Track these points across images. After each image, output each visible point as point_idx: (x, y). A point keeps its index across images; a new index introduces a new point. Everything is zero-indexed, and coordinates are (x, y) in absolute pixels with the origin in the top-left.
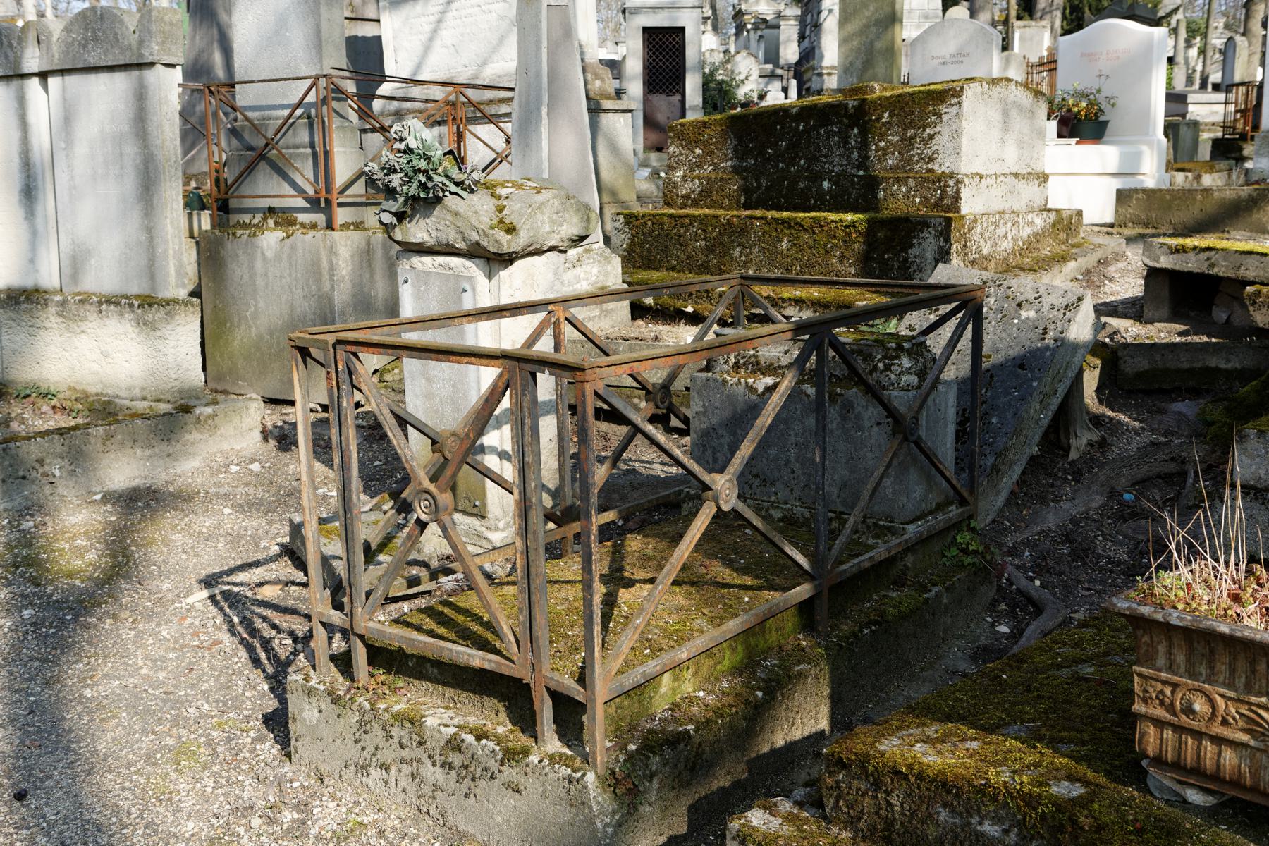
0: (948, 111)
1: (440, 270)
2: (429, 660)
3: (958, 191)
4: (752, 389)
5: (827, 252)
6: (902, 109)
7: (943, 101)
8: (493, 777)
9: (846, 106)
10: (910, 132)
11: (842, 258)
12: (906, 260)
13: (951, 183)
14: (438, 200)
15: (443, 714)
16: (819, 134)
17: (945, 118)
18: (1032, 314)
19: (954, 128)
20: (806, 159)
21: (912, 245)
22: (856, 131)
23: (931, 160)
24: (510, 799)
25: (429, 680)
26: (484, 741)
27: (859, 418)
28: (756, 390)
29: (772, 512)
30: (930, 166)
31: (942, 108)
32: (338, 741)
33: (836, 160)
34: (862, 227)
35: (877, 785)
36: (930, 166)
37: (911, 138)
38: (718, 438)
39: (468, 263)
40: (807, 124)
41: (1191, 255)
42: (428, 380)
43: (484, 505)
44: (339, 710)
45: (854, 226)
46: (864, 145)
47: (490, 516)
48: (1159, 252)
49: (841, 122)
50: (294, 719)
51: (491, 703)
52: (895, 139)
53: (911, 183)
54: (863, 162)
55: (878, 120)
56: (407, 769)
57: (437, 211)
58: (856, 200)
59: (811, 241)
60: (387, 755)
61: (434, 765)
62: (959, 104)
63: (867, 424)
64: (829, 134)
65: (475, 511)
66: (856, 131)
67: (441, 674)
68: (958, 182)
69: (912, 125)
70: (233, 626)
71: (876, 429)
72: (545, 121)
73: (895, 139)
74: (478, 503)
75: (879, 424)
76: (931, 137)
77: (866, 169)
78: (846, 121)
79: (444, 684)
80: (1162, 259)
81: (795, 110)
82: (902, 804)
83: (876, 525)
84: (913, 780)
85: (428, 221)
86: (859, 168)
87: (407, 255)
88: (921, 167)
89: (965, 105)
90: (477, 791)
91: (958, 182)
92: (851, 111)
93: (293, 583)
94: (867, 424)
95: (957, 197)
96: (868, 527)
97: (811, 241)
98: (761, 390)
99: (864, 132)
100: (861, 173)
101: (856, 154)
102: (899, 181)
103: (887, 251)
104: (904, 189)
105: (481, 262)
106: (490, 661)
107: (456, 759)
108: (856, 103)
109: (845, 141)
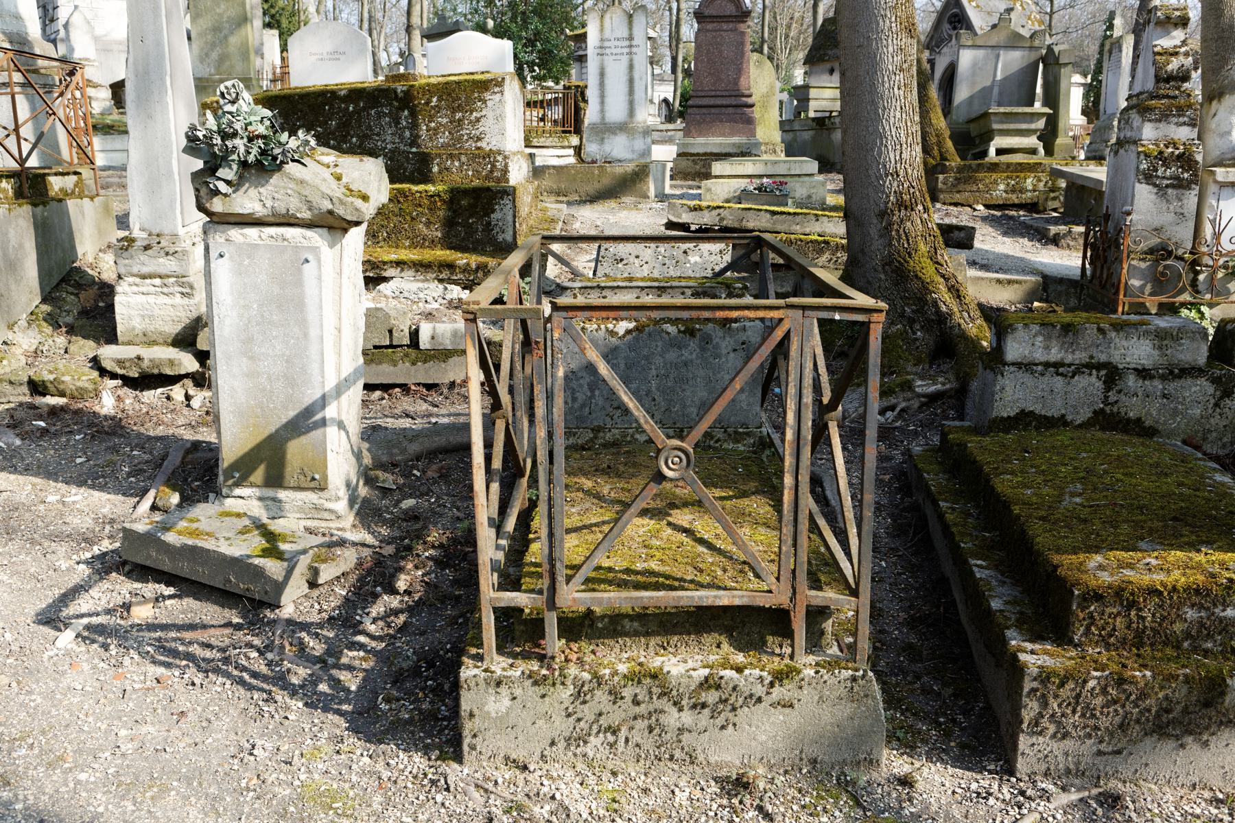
0: (492, 98)
1: (273, 242)
2: (627, 616)
3: (506, 165)
4: (612, 333)
5: (413, 219)
6: (449, 95)
7: (487, 89)
8: (759, 700)
9: (395, 91)
10: (458, 115)
11: (428, 224)
12: (489, 223)
13: (500, 158)
14: (279, 168)
15: (683, 663)
16: (369, 114)
17: (489, 103)
18: (697, 259)
19: (498, 112)
20: (358, 136)
21: (493, 211)
22: (406, 112)
23: (479, 139)
24: (779, 715)
25: (627, 634)
26: (747, 672)
27: (717, 347)
28: (617, 333)
29: (637, 436)
30: (479, 144)
31: (487, 96)
32: (540, 723)
33: (389, 138)
34: (446, 197)
35: (1132, 604)
36: (479, 144)
37: (459, 120)
38: (577, 380)
39: (309, 233)
40: (356, 105)
41: (706, 212)
42: (251, 358)
43: (325, 477)
44: (541, 690)
45: (439, 196)
46: (414, 126)
47: (330, 487)
48: (681, 211)
49: (391, 105)
50: (472, 715)
51: (709, 639)
52: (445, 120)
53: (463, 158)
54: (414, 141)
55: (427, 103)
56: (641, 724)
57: (275, 179)
58: (412, 173)
59: (396, 210)
60: (615, 716)
61: (681, 710)
62: (502, 92)
63: (724, 351)
64: (380, 115)
65: (313, 485)
66: (406, 112)
67: (642, 626)
68: (505, 158)
69: (459, 108)
70: (152, 657)
71: (732, 355)
72: (170, 92)
73: (445, 120)
74: (317, 477)
75: (735, 350)
76: (478, 120)
77: (419, 146)
78: (396, 104)
79: (647, 634)
80: (684, 215)
81: (343, 93)
82: (1154, 615)
83: (736, 432)
84: (1166, 594)
85: (261, 190)
86: (411, 145)
87: (221, 227)
88: (471, 145)
89: (506, 93)
90: (736, 720)
91: (505, 158)
92: (401, 95)
93: (164, 598)
94: (724, 351)
95: (505, 171)
96: (730, 435)
97: (396, 210)
98: (621, 333)
99: (413, 114)
100: (414, 150)
101: (407, 134)
102: (451, 157)
103: (471, 216)
104: (457, 164)
105: (324, 231)
106: (1149, 569)
107: (711, 697)
108: (405, 88)
109: (397, 121)
